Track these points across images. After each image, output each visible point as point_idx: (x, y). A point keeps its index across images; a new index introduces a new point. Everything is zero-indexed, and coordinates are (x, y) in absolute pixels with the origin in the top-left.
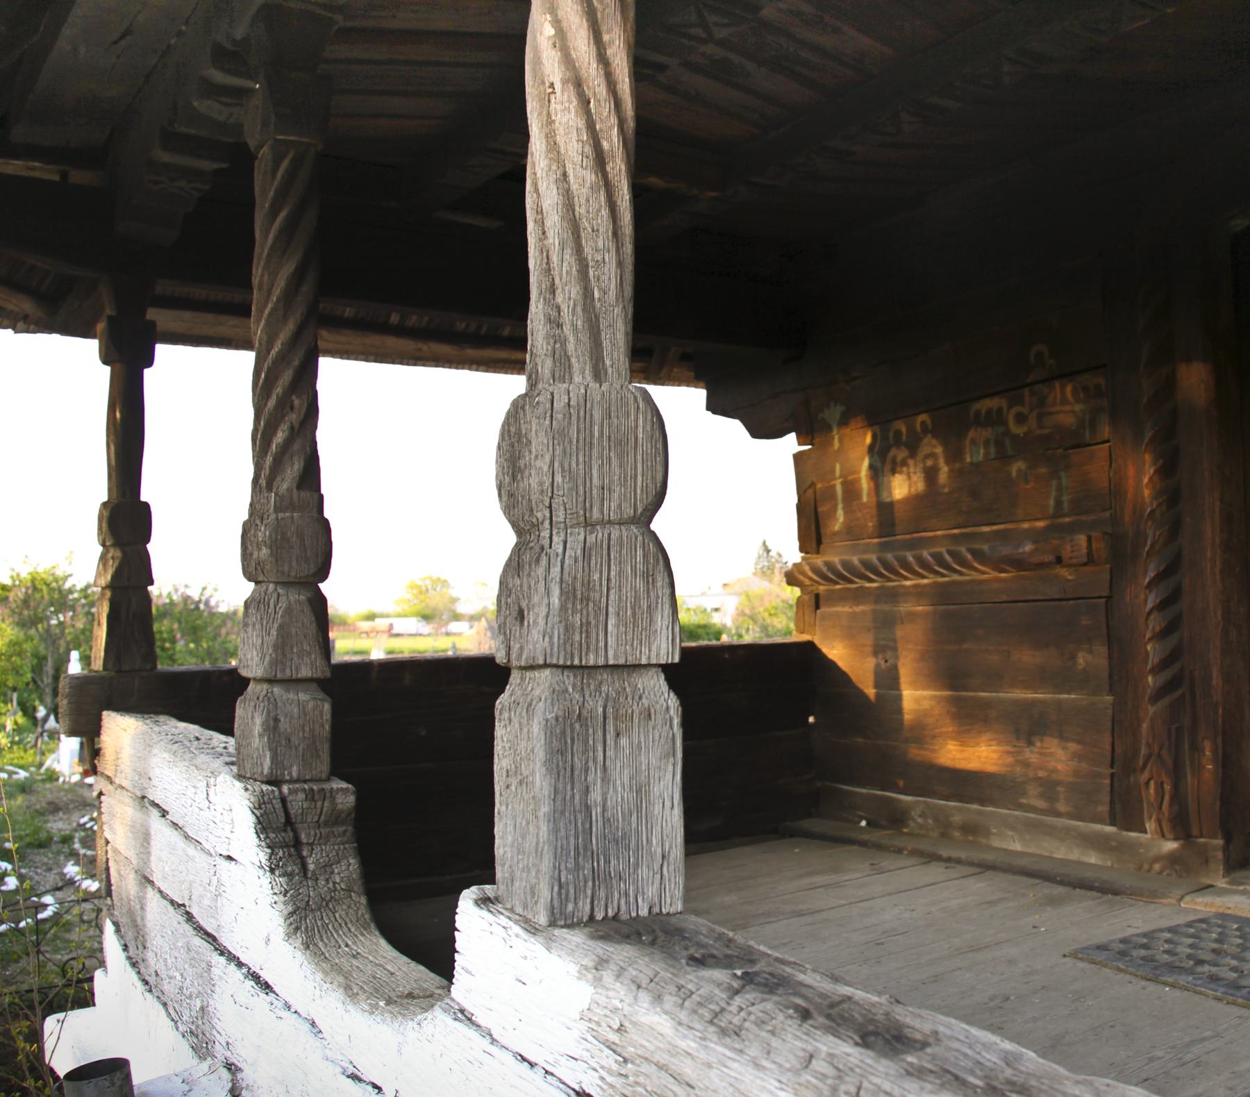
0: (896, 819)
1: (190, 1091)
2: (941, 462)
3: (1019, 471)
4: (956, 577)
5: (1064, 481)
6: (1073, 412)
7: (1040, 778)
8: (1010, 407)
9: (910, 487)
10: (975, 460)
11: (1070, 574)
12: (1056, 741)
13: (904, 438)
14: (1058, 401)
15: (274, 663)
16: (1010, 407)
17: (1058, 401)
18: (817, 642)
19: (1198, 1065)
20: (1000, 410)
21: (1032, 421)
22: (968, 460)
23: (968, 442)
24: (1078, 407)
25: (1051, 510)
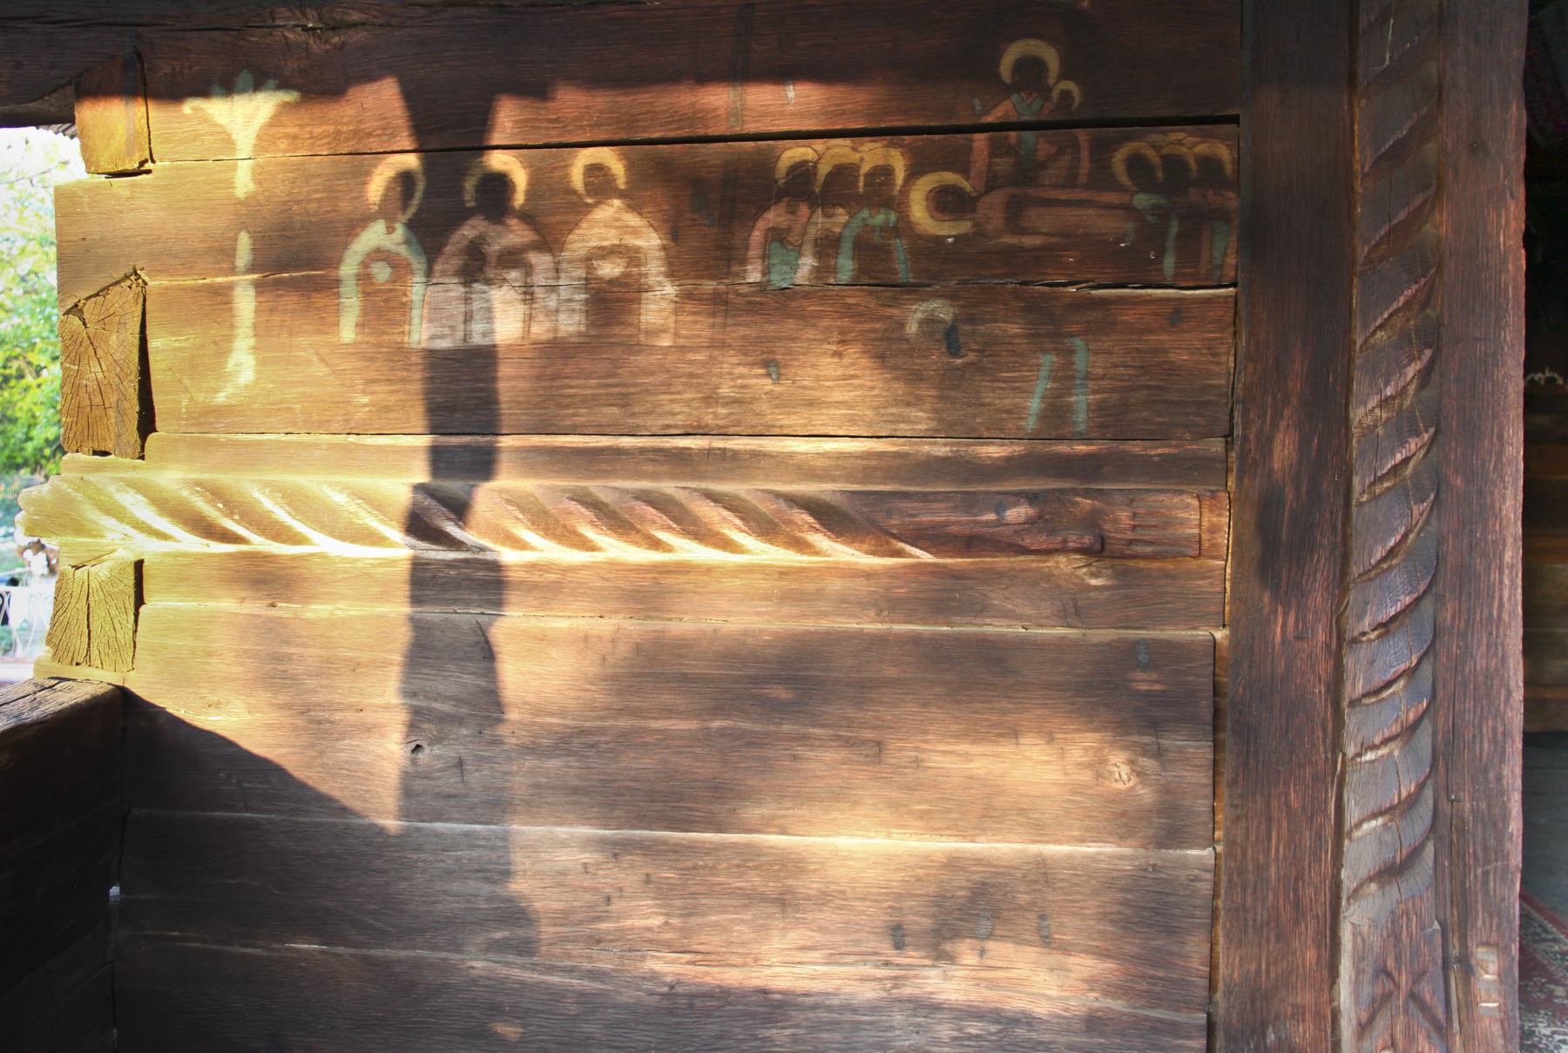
0: (515, 811)
1: (35, 404)
2: (654, 269)
3: (929, 322)
4: (688, 550)
5: (1080, 361)
6: (1128, 209)
7: (970, 1037)
8: (914, 173)
9: (529, 319)
10: (777, 280)
11: (1095, 575)
12: (1031, 953)
13: (519, 199)
14: (1082, 180)
15: (421, 145)
16: (914, 173)
17: (1082, 180)
18: (141, 686)
19: (1046, 882)
20: (885, 172)
21: (992, 211)
22: (754, 276)
23: (757, 236)
24: (1142, 200)
25: (1031, 424)
